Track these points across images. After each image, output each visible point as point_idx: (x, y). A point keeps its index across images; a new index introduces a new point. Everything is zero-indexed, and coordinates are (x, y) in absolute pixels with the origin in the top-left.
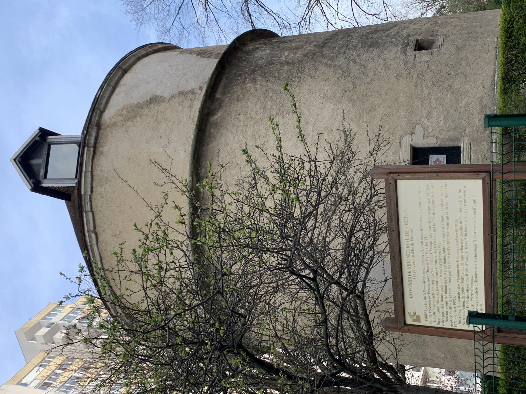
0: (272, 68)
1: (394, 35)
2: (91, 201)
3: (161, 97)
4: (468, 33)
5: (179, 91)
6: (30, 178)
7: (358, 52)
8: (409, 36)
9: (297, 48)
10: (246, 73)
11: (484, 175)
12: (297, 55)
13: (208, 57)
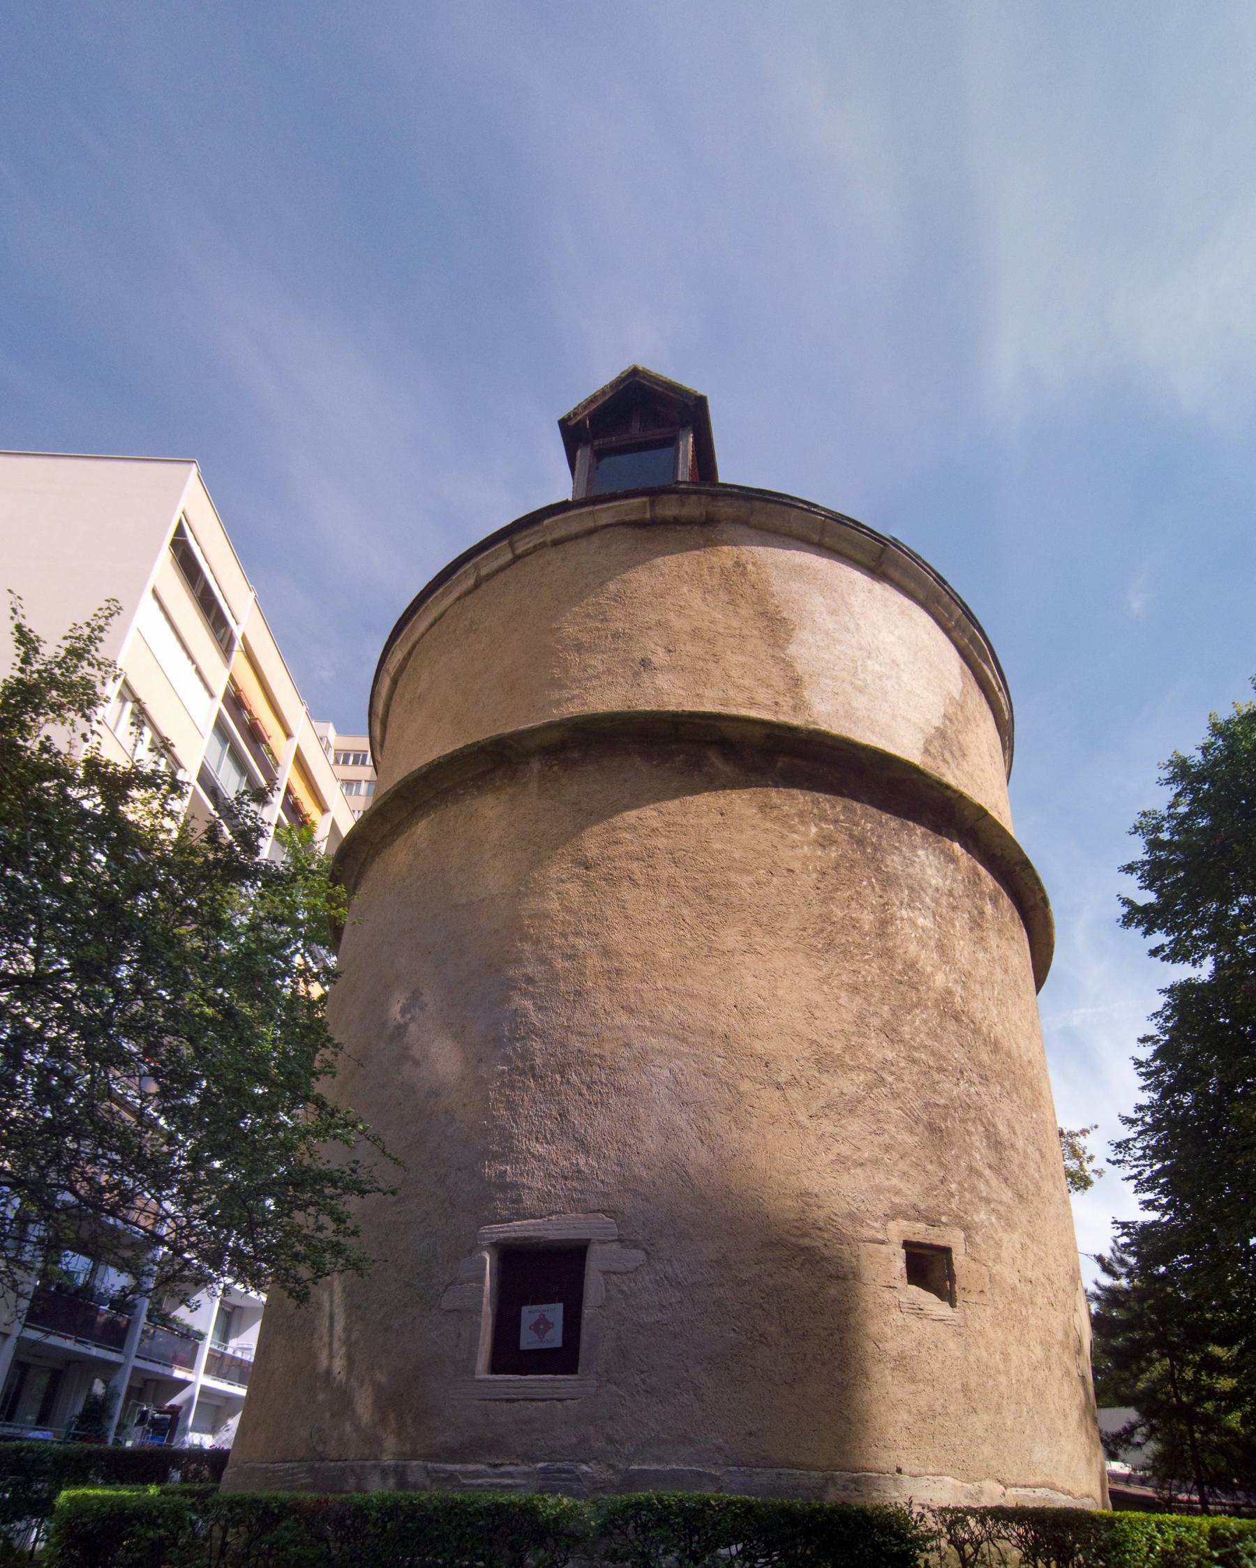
0: (870, 883)
1: (973, 1189)
3: (787, 640)
4: (965, 1389)
5: (806, 678)
6: (594, 416)
8: (966, 1228)
12: (913, 948)
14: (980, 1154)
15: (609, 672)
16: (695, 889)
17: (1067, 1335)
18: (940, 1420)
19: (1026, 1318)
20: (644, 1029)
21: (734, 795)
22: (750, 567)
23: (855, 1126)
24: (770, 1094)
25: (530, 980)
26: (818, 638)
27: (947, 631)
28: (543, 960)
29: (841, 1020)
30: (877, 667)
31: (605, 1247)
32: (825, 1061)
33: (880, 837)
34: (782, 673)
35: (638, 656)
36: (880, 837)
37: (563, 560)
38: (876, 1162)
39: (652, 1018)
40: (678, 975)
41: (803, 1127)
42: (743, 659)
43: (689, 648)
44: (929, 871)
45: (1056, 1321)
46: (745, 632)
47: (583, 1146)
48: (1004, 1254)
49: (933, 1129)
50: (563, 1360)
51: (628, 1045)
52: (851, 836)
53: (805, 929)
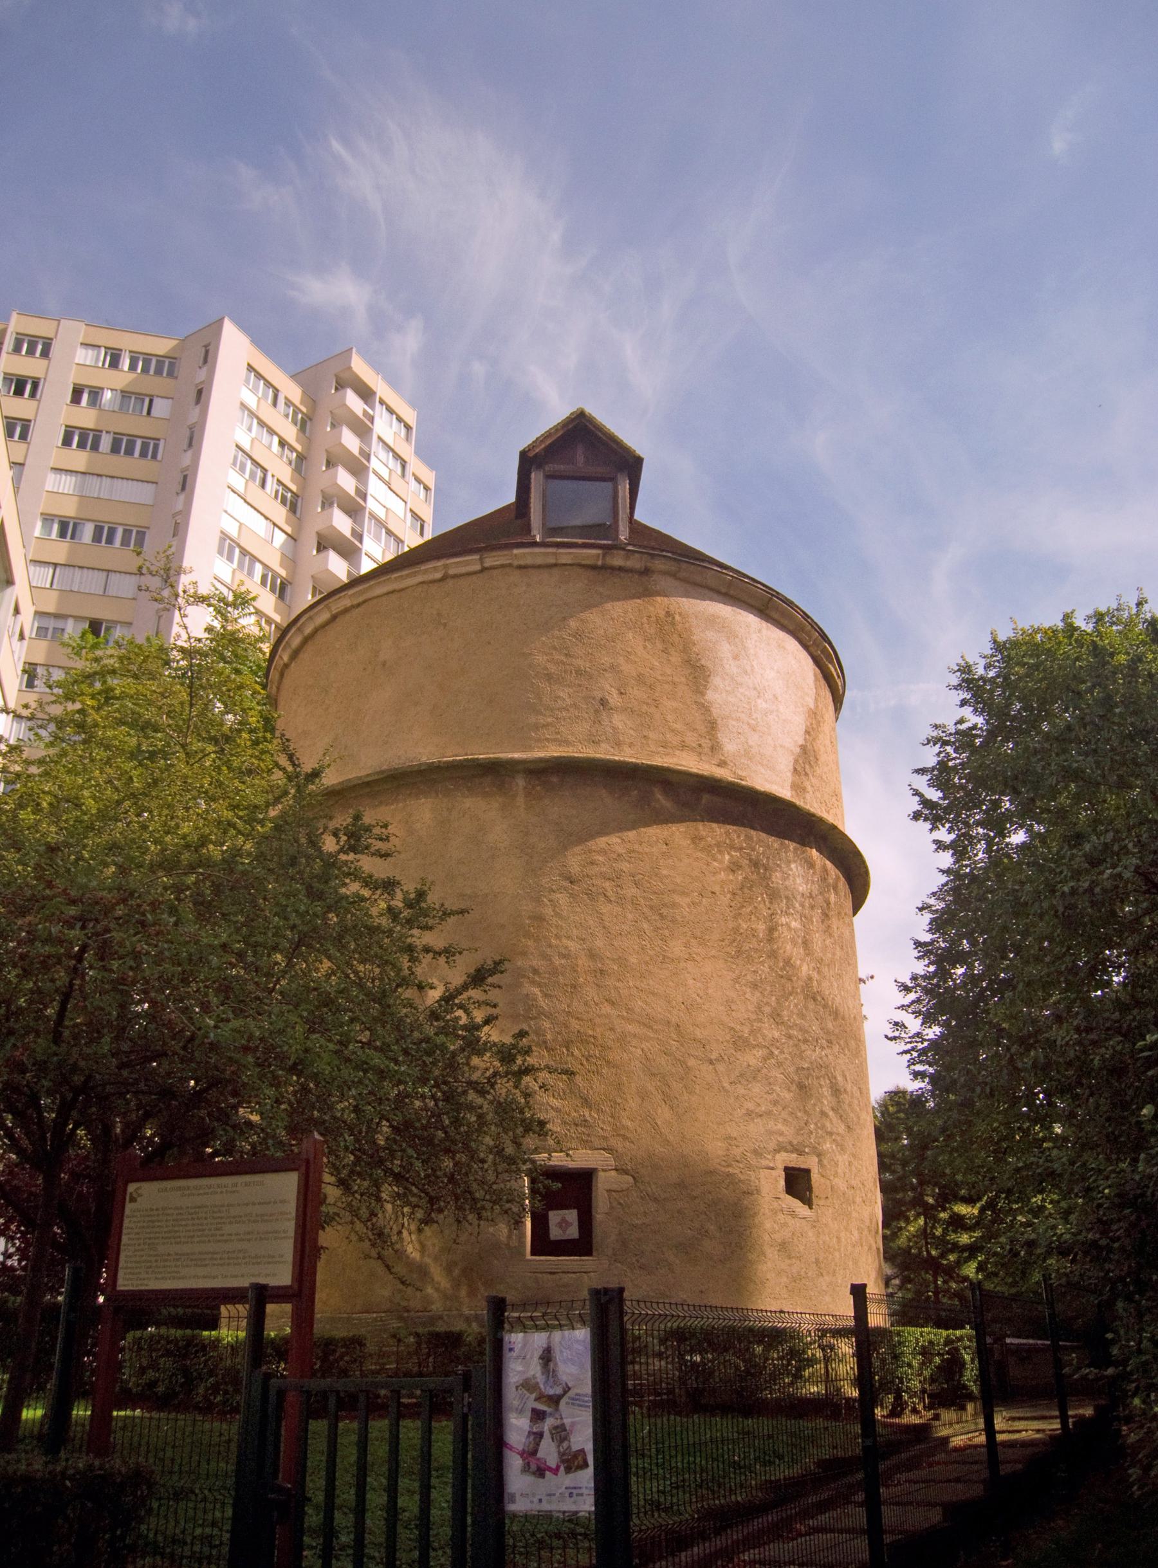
1: (823, 1127)
2: (502, 566)
4: (817, 1261)
5: (719, 721)
7: (788, 1063)
8: (819, 1155)
9: (806, 943)
10: (753, 850)
11: (296, 1286)
12: (789, 947)
13: (795, 769)
14: (827, 1101)
15: (575, 705)
16: (651, 908)
17: (871, 1221)
18: (803, 1281)
19: (850, 1213)
20: (623, 1018)
21: (674, 828)
22: (677, 617)
23: (757, 1088)
24: (706, 1068)
25: (536, 971)
26: (727, 682)
27: (806, 647)
28: (545, 957)
29: (748, 1010)
30: (764, 705)
31: (607, 1174)
32: (740, 1043)
33: (768, 858)
34: (703, 717)
35: (598, 694)
36: (768, 858)
37: (528, 585)
38: (769, 1113)
39: (628, 1010)
40: (642, 976)
41: (727, 1091)
42: (675, 704)
43: (636, 692)
44: (798, 881)
45: (866, 1215)
46: (676, 679)
47: (586, 1102)
48: (839, 1171)
49: (801, 1087)
50: (582, 1245)
51: (612, 1029)
52: (750, 860)
53: (723, 940)
